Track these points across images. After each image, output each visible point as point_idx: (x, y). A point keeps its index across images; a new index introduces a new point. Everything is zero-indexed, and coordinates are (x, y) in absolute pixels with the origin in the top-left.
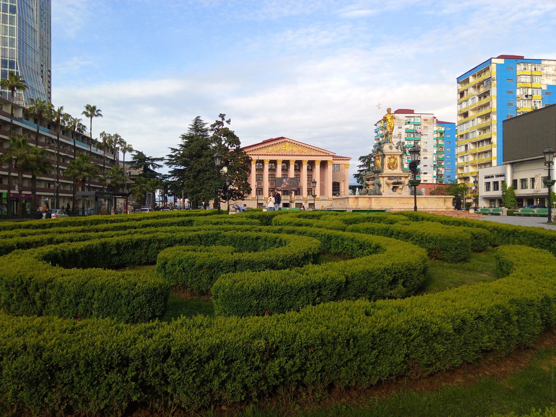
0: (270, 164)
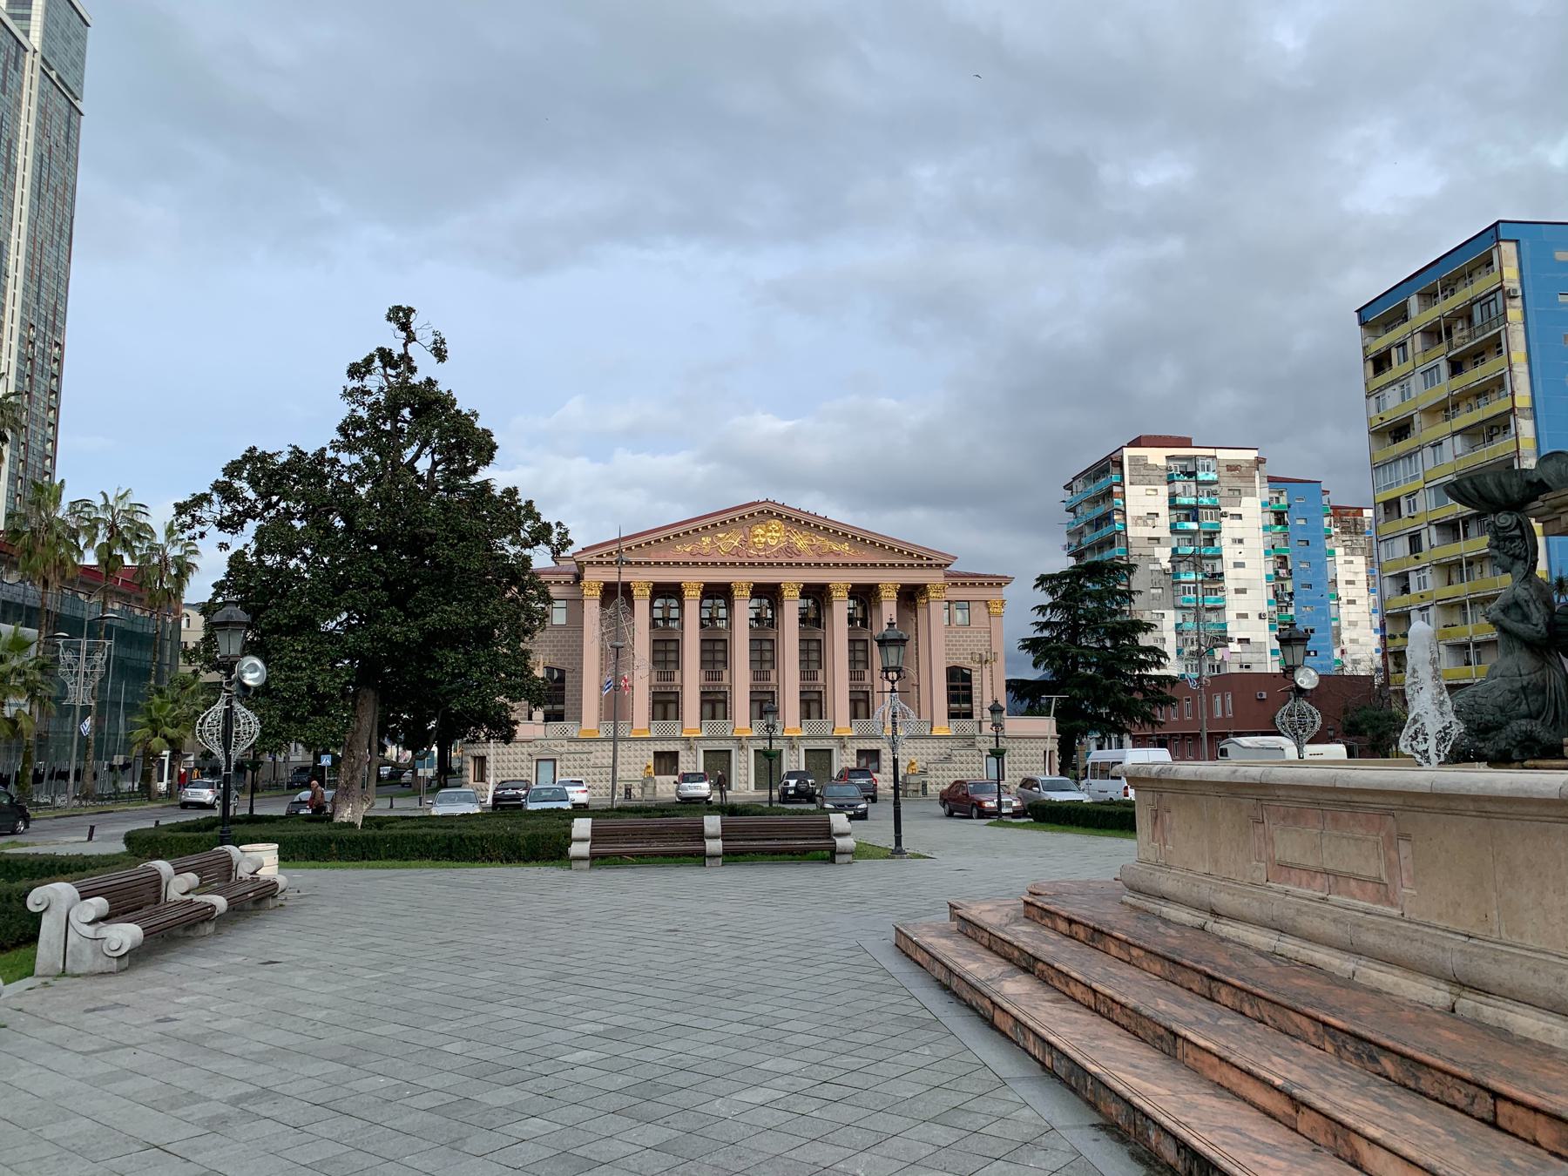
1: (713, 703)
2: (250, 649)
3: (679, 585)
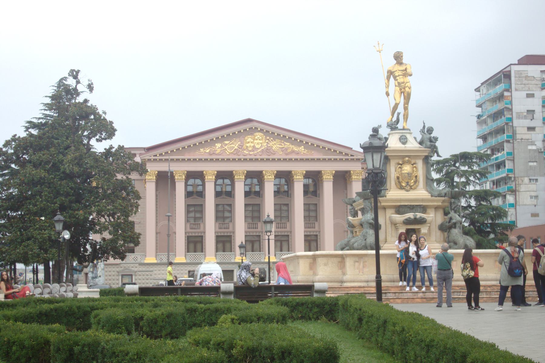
0: (249, 181)
1: (224, 243)
2: (65, 228)
3: (202, 172)
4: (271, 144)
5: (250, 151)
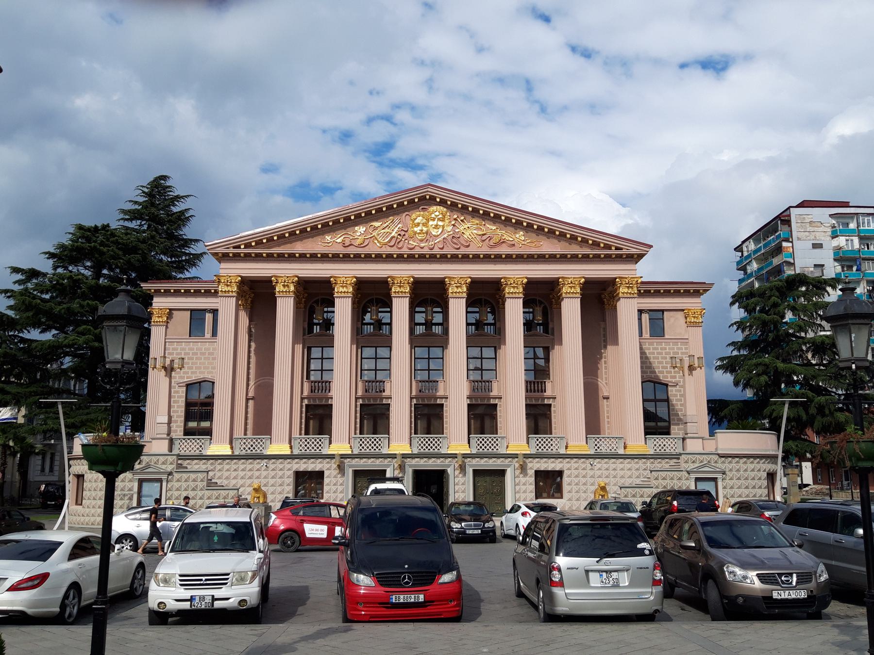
4: (462, 227)
5: (421, 241)
